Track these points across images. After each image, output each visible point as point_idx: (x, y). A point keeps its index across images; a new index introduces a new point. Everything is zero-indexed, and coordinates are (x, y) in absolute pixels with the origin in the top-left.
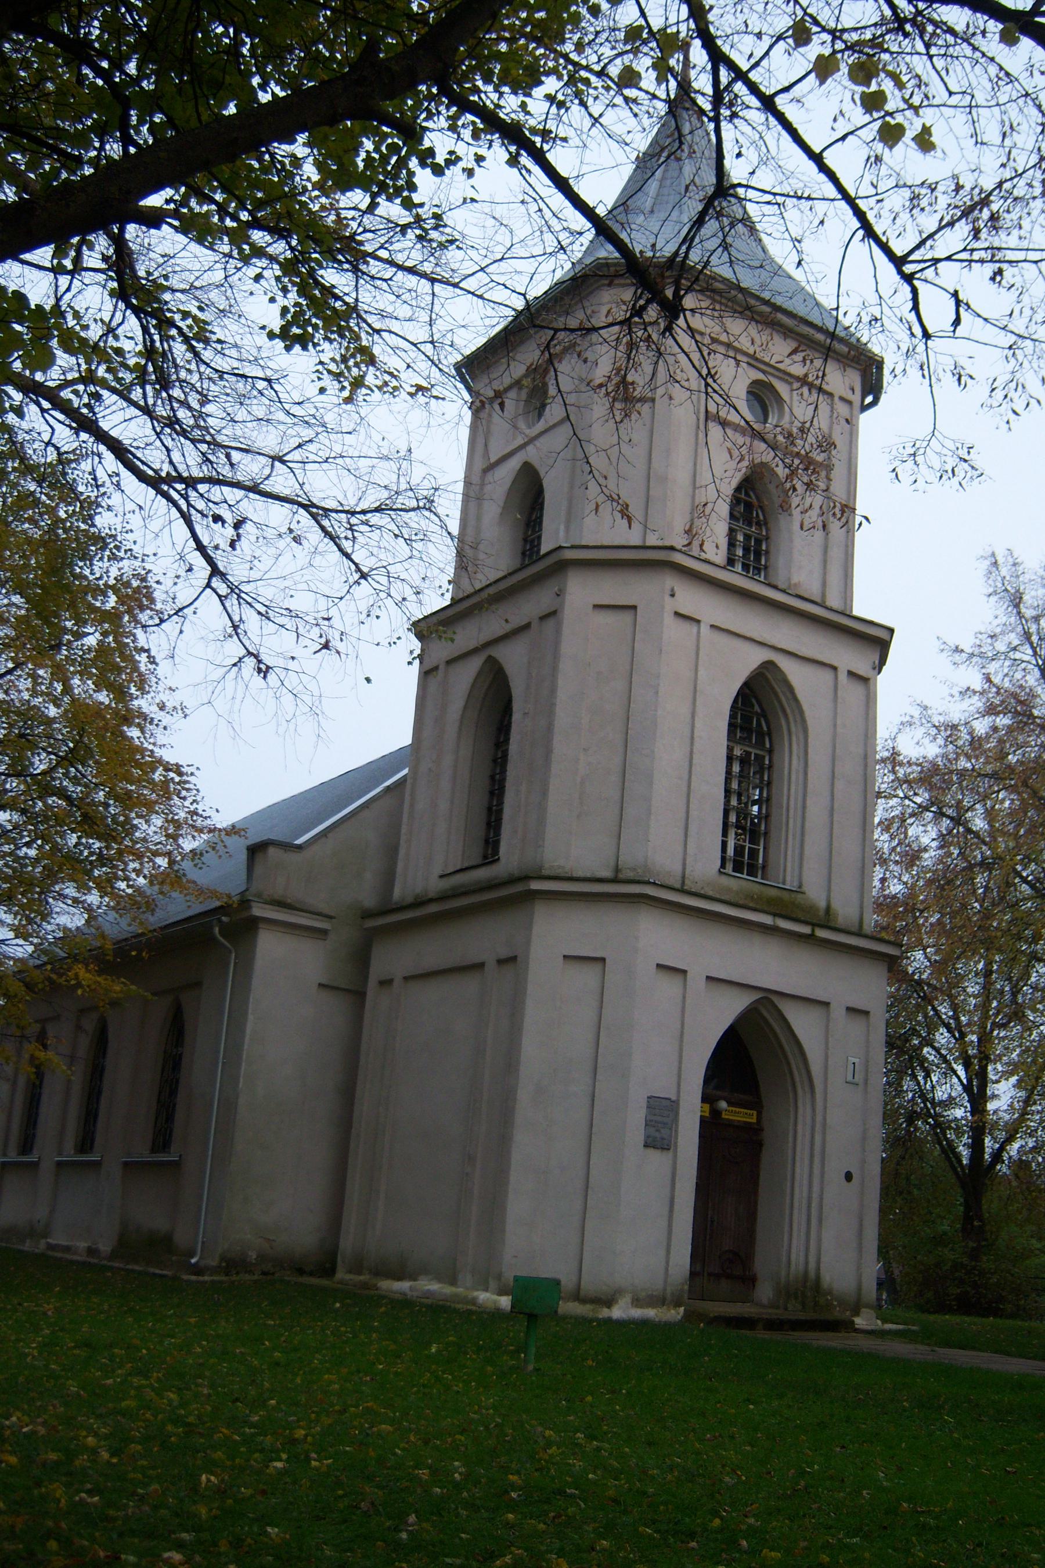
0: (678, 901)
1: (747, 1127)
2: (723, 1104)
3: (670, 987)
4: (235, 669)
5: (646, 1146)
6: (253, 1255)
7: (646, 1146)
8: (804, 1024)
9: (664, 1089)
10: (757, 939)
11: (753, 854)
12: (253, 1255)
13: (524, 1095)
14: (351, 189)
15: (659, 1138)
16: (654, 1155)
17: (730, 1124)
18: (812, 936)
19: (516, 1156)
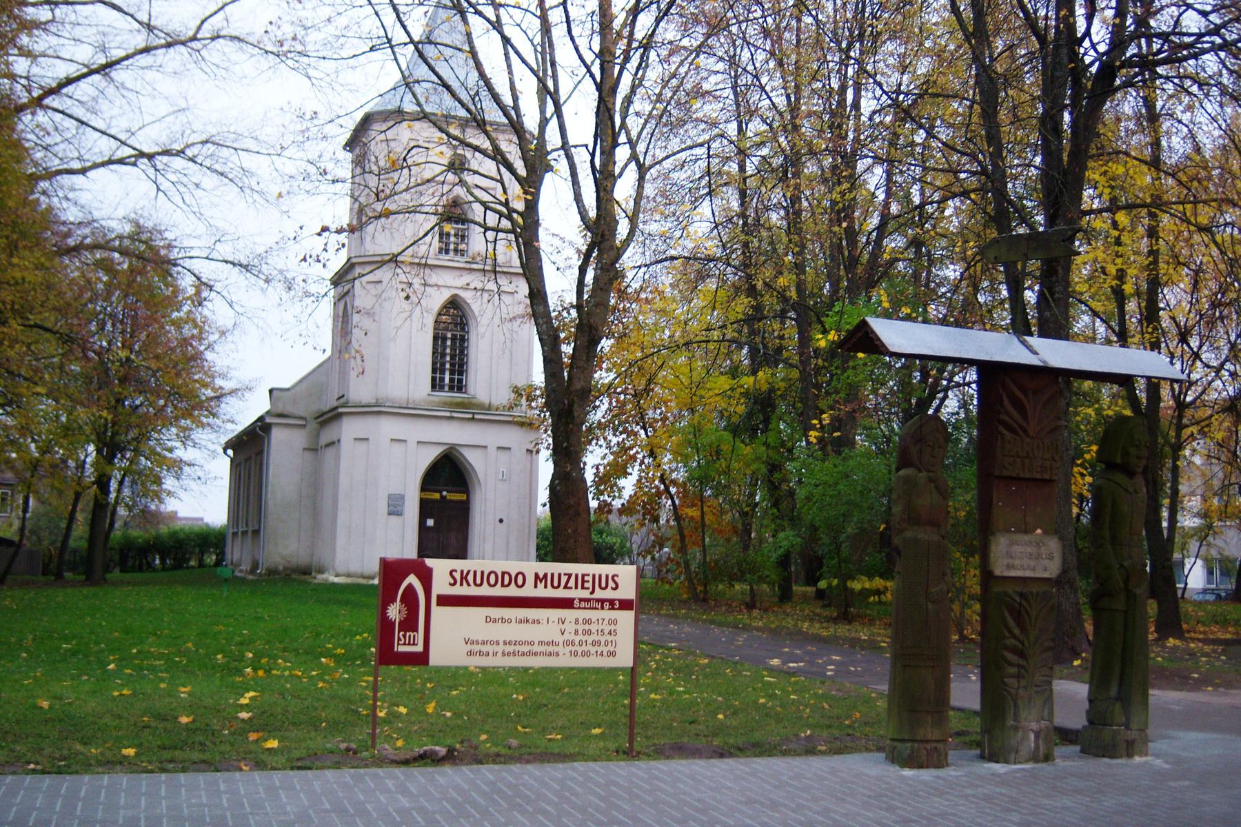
0: (407, 412)
1: (462, 502)
2: (444, 493)
3: (398, 447)
4: (235, 305)
5: (390, 514)
6: (281, 568)
7: (390, 514)
8: (473, 458)
9: (396, 490)
10: (445, 423)
11: (460, 381)
12: (281, 568)
13: (341, 497)
14: (17, 144)
15: (395, 509)
16: (394, 519)
17: (451, 501)
18: (473, 419)
19: (339, 522)
